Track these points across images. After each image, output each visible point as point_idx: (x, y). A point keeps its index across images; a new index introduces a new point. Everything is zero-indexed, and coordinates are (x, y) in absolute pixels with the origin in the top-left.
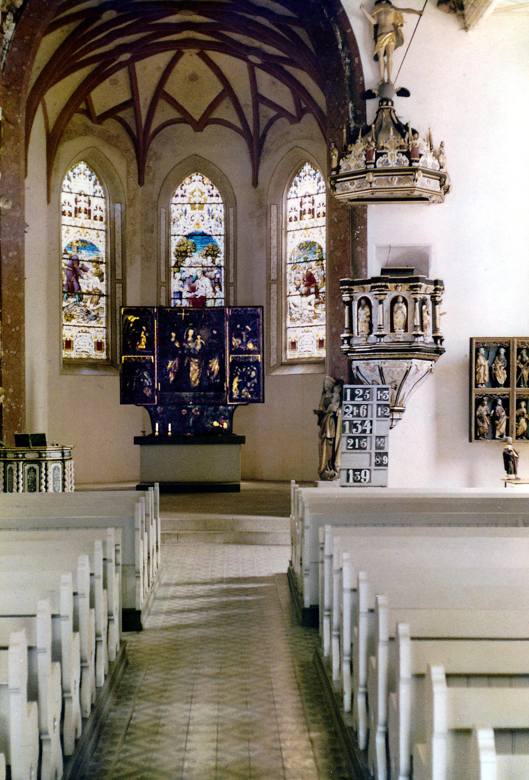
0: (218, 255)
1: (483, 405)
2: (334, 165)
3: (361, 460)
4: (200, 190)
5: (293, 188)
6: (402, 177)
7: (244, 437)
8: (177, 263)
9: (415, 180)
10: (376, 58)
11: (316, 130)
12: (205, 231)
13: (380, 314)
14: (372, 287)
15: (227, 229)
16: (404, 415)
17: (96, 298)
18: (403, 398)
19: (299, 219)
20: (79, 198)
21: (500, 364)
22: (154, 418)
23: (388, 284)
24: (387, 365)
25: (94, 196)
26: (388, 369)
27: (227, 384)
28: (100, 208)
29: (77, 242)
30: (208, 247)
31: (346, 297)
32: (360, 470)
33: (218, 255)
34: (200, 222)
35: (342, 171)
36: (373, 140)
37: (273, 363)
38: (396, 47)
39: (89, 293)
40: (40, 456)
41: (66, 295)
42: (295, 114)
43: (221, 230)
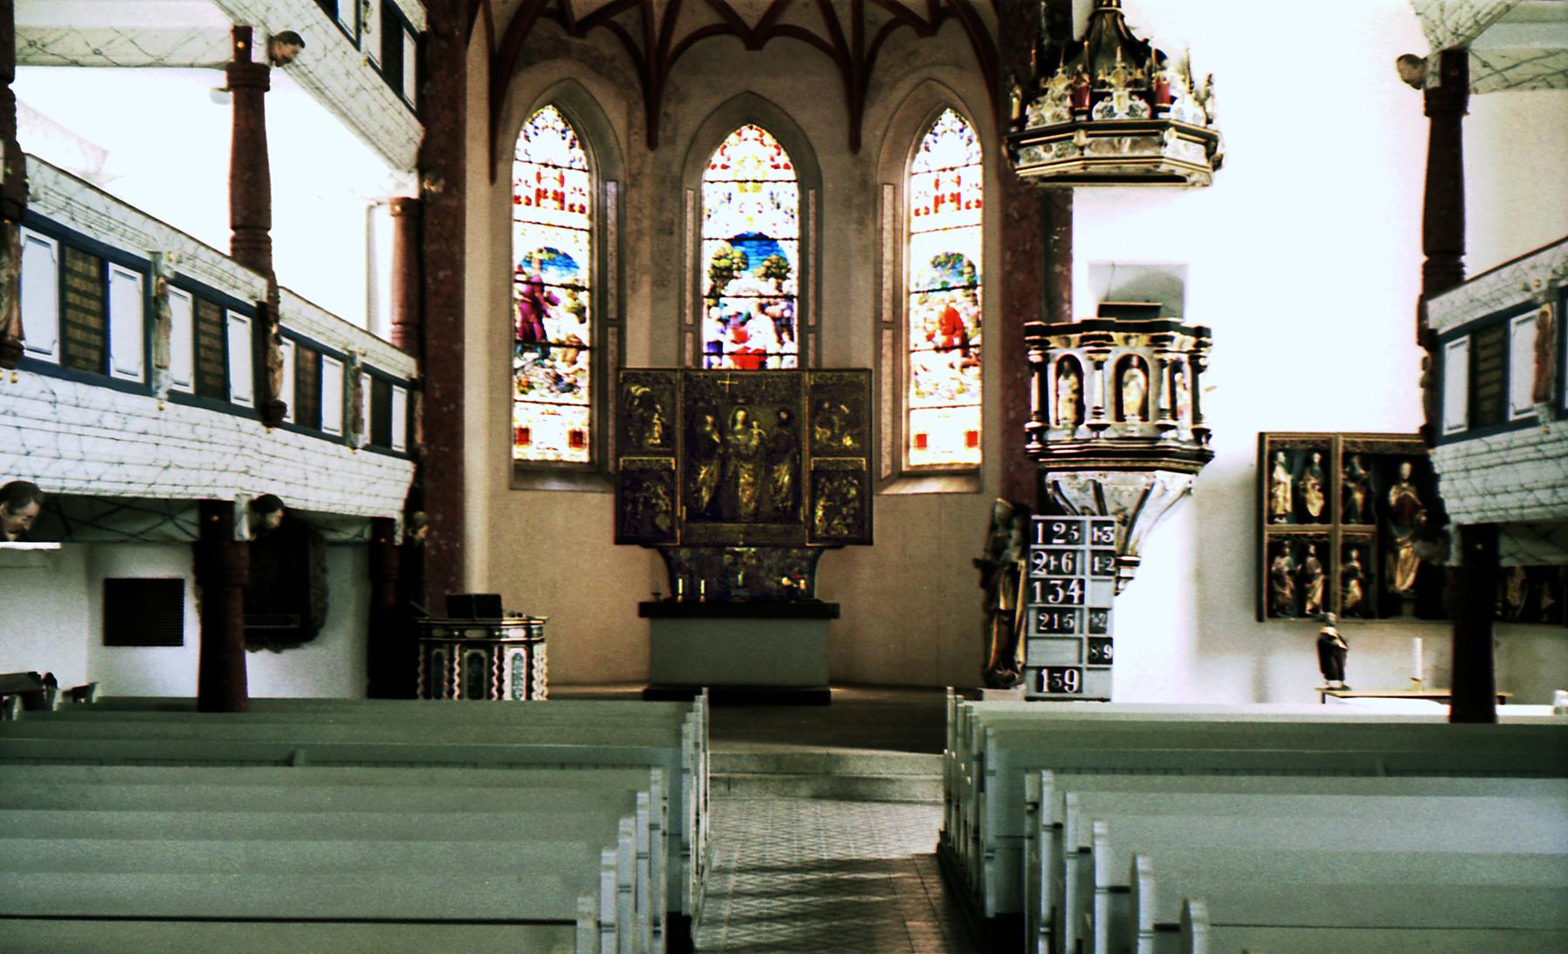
1: (1283, 555)
3: (1063, 652)
5: (922, 154)
7: (836, 606)
8: (713, 289)
9: (1163, 144)
11: (966, 50)
13: (1098, 388)
14: (1083, 339)
15: (803, 226)
16: (1137, 572)
17: (571, 352)
21: (1313, 481)
22: (673, 572)
23: (1112, 334)
24: (1110, 480)
26: (1112, 487)
27: (803, 513)
31: (1035, 356)
32: (1062, 670)
35: (1030, 126)
36: (1085, 70)
37: (886, 471)
39: (560, 344)
40: (491, 634)
42: (926, 18)
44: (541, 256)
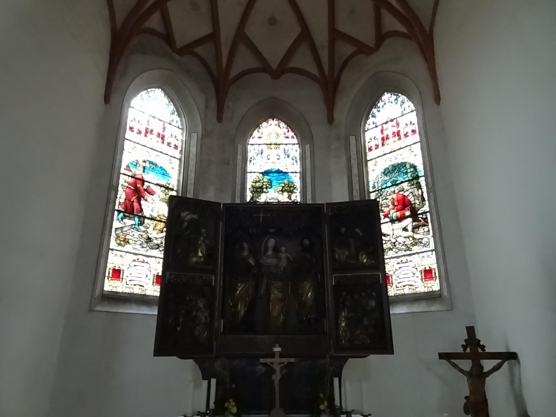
0: (294, 191)
5: (371, 120)
12: (281, 169)
25: (170, 124)
28: (176, 137)
29: (145, 162)
30: (284, 183)
33: (294, 191)
39: (152, 219)
41: (121, 215)
44: (144, 164)
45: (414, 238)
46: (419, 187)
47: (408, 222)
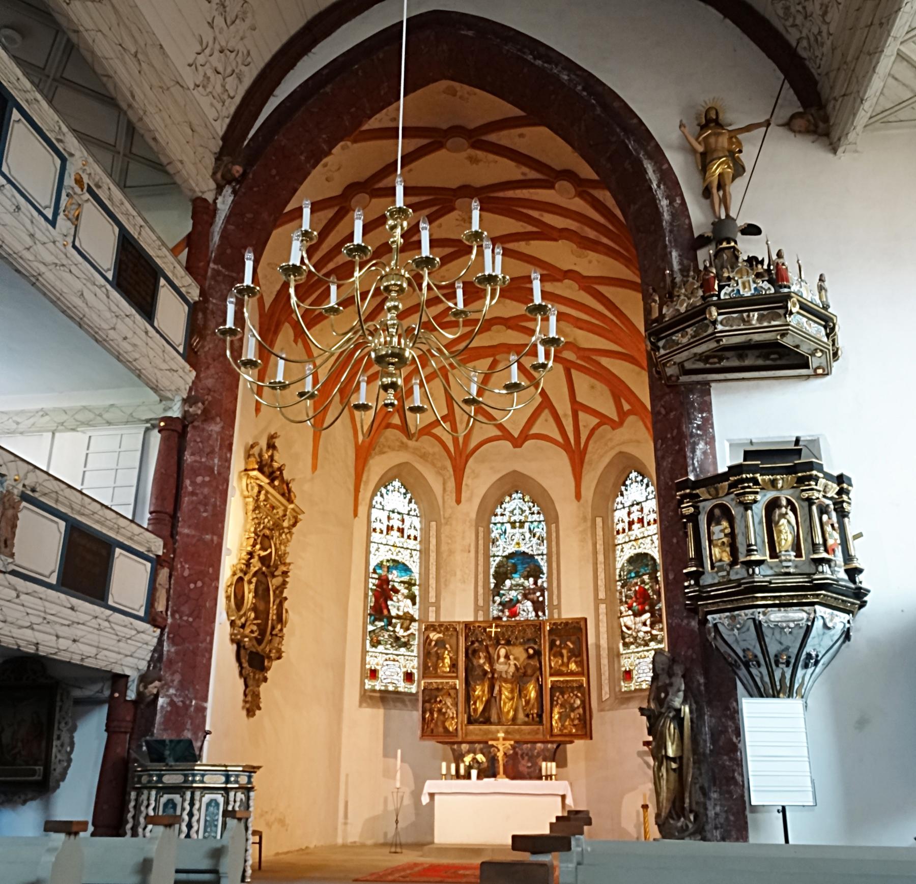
2: (655, 314)
4: (520, 508)
5: (619, 499)
6: (765, 312)
10: (707, 193)
12: (526, 551)
18: (802, 684)
19: (627, 530)
20: (392, 515)
29: (388, 561)
31: (687, 509)
34: (521, 541)
38: (733, 179)
39: (398, 617)
42: (616, 418)
43: (544, 549)
45: (652, 635)
46: (657, 582)
47: (647, 616)
